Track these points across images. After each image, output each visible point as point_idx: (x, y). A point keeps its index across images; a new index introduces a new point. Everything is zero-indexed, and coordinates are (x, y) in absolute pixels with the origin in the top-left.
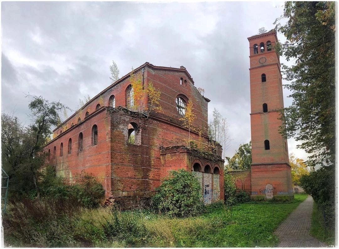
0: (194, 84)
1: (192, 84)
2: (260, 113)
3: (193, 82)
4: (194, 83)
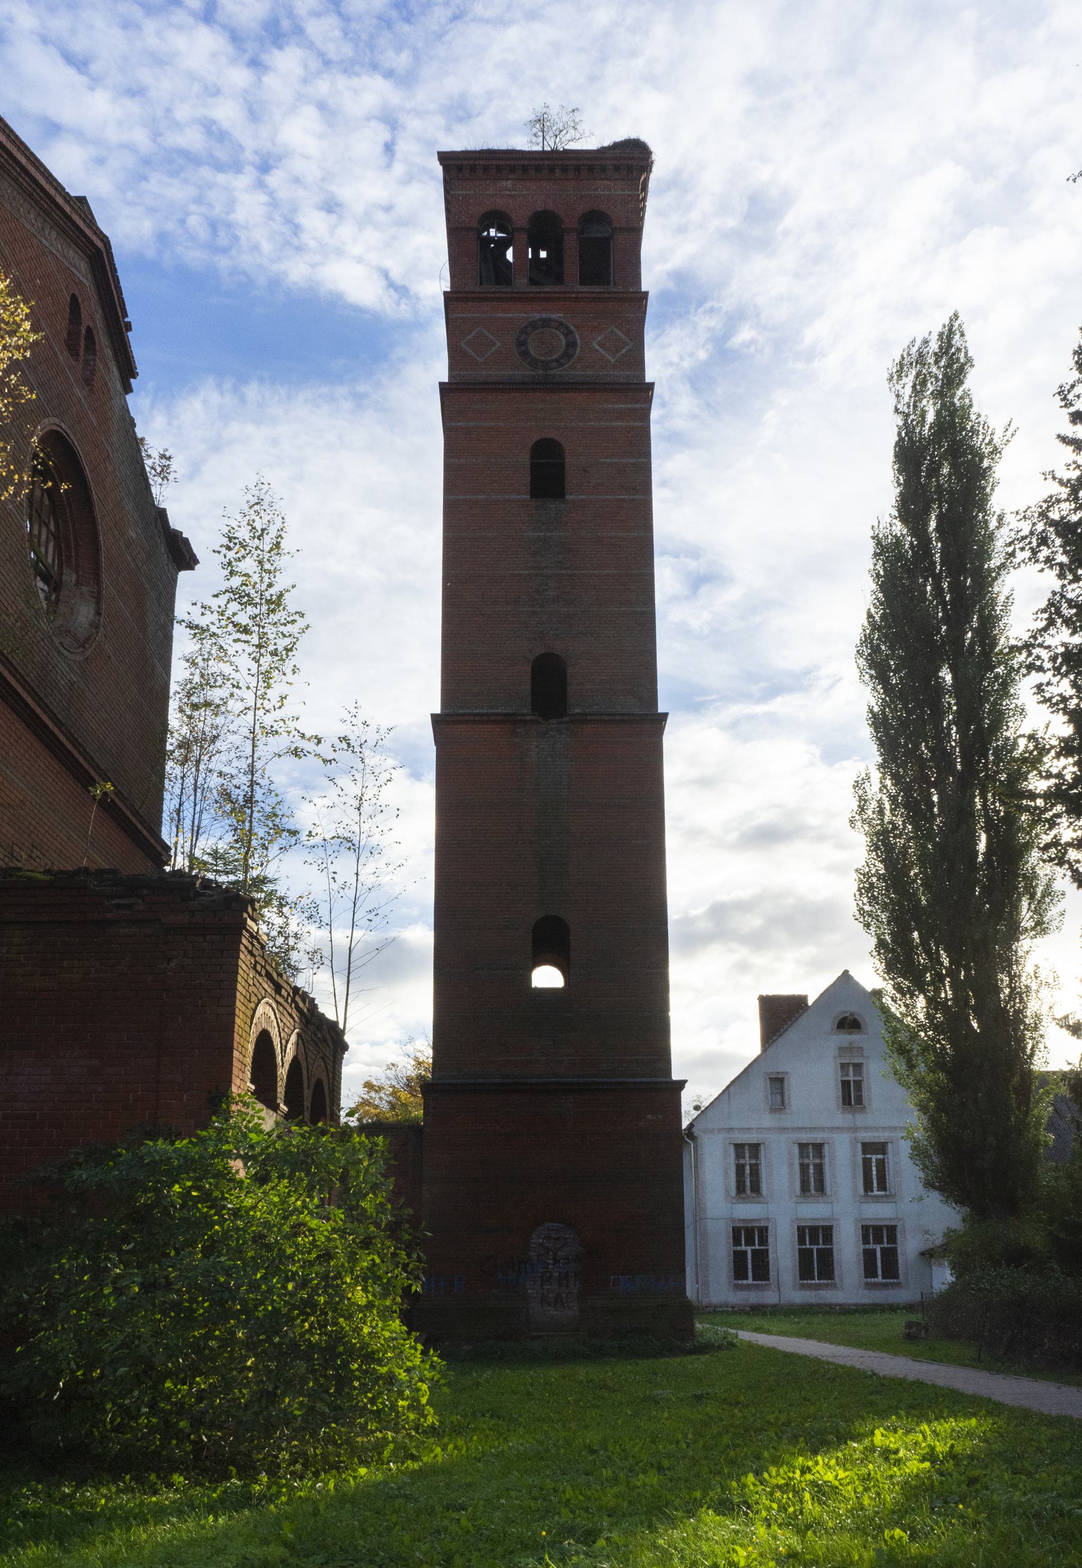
0: (128, 389)
1: (119, 386)
2: (508, 719)
3: (128, 370)
4: (134, 375)
